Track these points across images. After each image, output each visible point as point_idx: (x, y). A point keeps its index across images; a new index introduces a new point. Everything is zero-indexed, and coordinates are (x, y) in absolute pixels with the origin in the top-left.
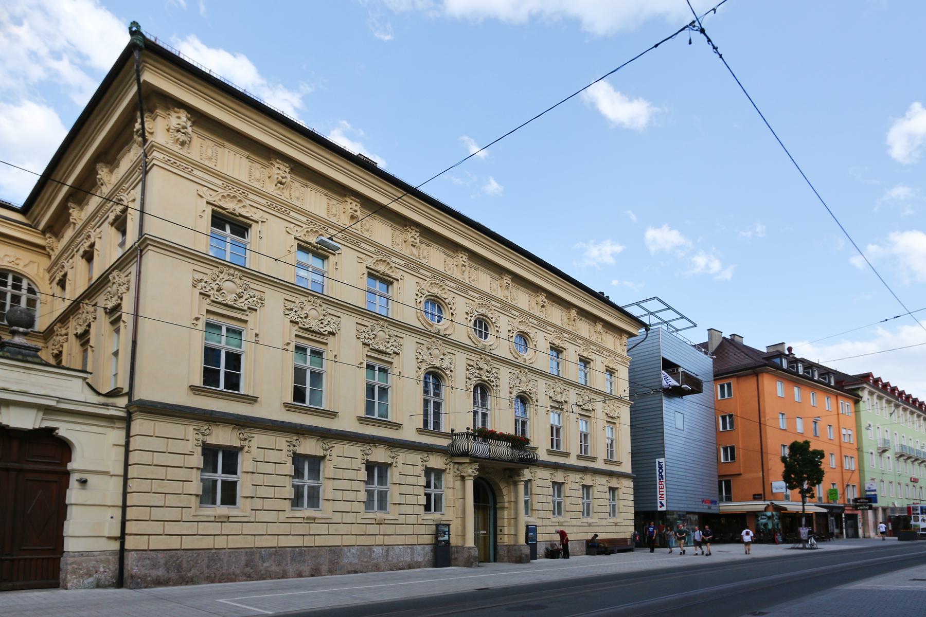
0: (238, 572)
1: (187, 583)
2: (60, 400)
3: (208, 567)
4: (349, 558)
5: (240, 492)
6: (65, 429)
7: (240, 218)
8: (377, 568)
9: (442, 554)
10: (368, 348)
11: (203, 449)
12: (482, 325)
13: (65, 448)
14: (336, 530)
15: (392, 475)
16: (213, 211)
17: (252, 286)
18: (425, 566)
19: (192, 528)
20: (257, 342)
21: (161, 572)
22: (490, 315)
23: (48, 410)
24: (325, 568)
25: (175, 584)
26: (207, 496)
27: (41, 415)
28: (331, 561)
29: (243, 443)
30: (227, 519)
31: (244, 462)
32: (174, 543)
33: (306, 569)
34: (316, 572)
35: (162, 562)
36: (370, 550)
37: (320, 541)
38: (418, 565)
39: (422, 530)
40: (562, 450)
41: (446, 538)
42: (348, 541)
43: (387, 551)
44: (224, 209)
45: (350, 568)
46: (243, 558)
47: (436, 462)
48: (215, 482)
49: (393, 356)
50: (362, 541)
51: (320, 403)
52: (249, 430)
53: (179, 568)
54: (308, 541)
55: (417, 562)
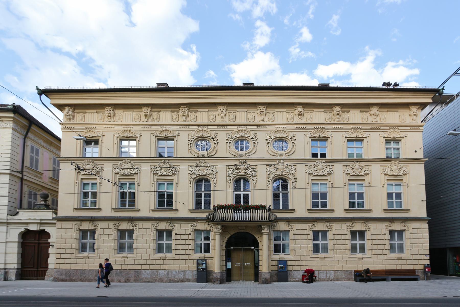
0: (92, 278)
1: (73, 281)
2: (41, 220)
3: (80, 276)
4: (145, 275)
5: (367, 248)
6: (48, 229)
7: (94, 138)
8: (161, 280)
9: (204, 275)
10: (349, 176)
11: (351, 232)
12: (240, 142)
13: (48, 235)
14: (138, 262)
15: (405, 235)
16: (386, 140)
17: (98, 164)
18: (193, 281)
19: (75, 261)
20: (370, 186)
21: (63, 277)
22: (246, 135)
23: (41, 224)
24: (132, 279)
25: (69, 281)
26: (354, 249)
27: (39, 225)
28: (135, 276)
29: (210, 228)
30: (399, 259)
31: (367, 235)
32: (68, 267)
33: (123, 279)
34: (127, 280)
35: (64, 273)
36: (157, 272)
37: (129, 267)
38: (189, 281)
39: (191, 262)
40: (403, 208)
41: (204, 267)
42: (144, 267)
43: (168, 273)
44: (316, 137)
45: (145, 280)
46: (94, 273)
47: (201, 226)
48: (201, 244)
49: (328, 176)
50: (152, 267)
51: (363, 207)
52: (96, 222)
53: (70, 275)
54: (124, 267)
55: (187, 279)
